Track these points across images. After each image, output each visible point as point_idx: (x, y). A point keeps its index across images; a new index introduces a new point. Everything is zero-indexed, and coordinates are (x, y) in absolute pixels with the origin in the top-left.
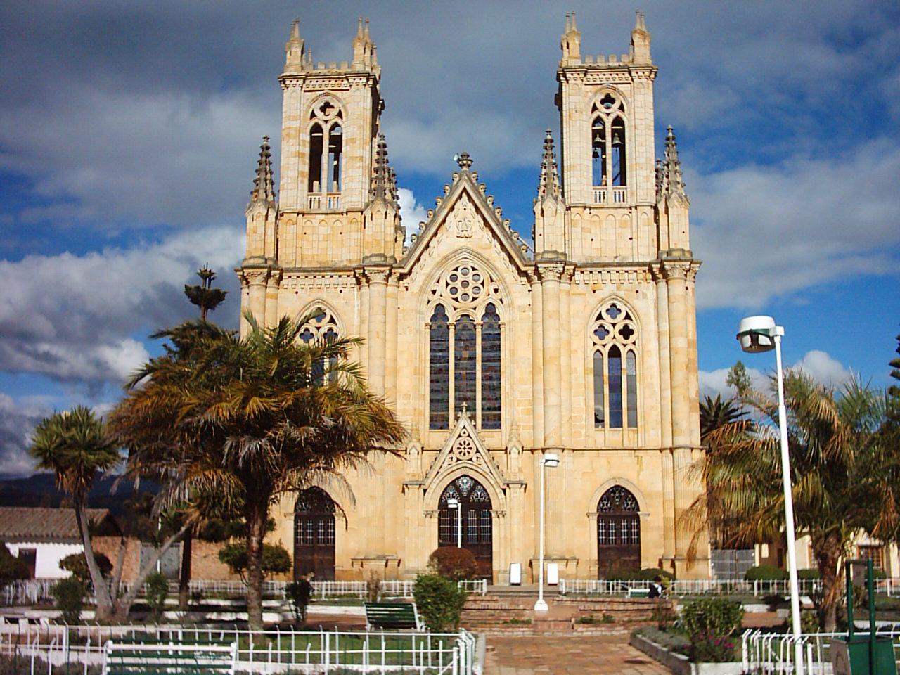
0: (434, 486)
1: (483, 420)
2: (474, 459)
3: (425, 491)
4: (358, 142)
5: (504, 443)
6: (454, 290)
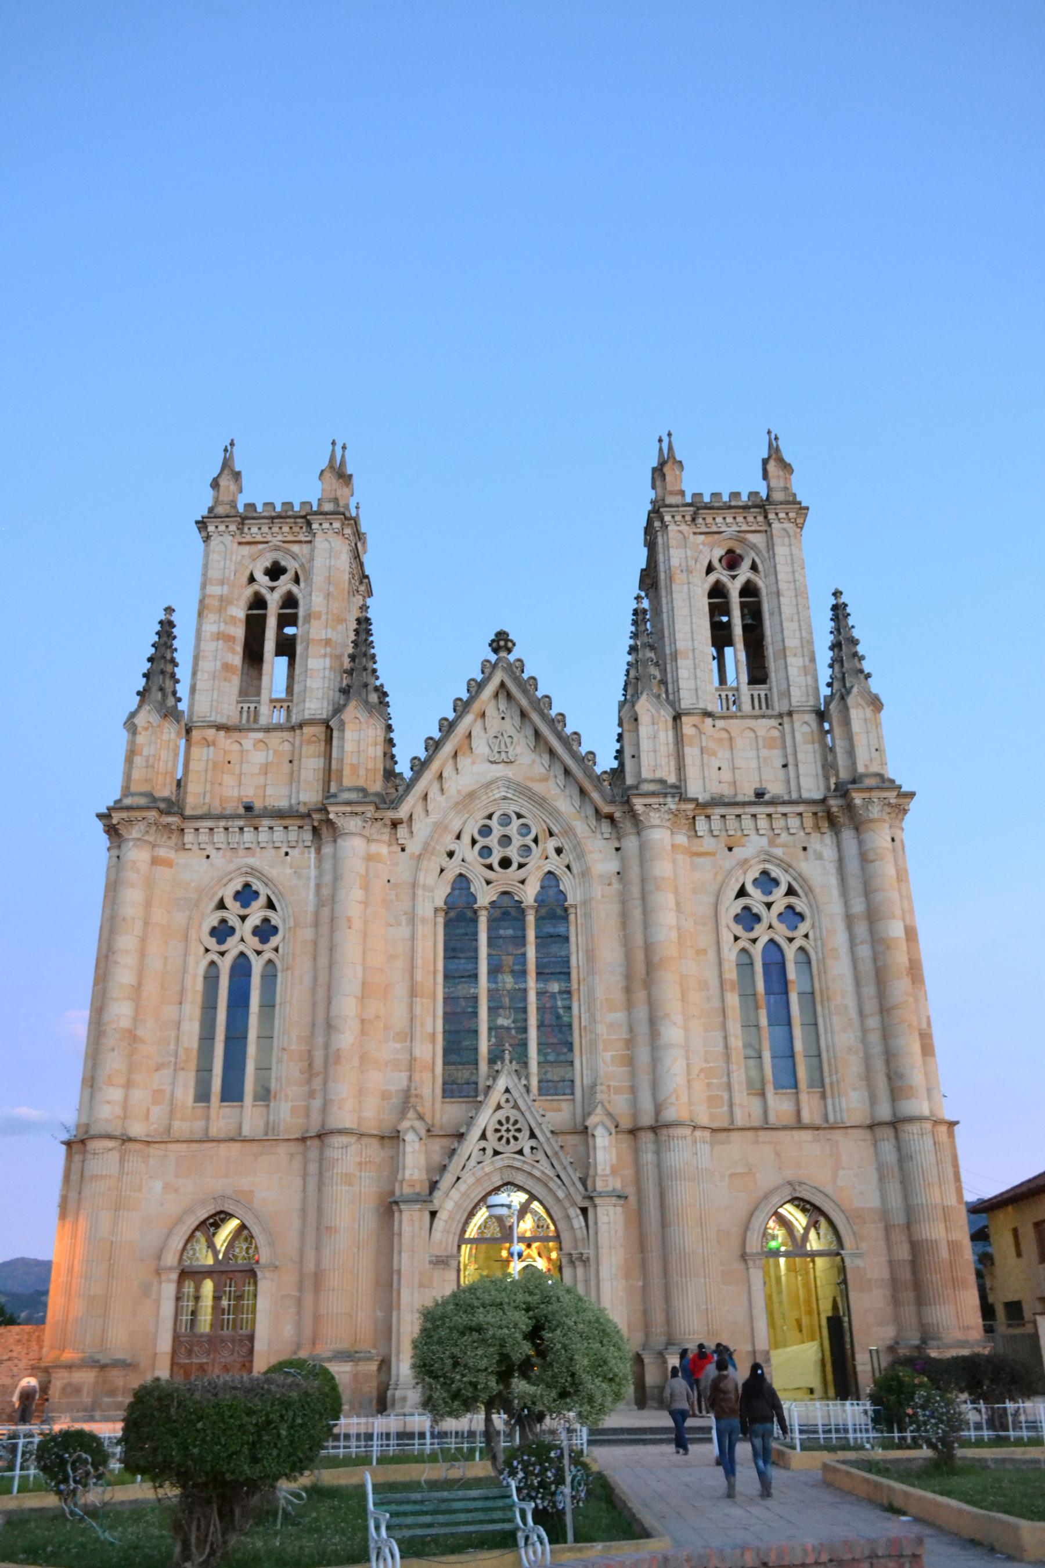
0: (449, 1205)
1: (524, 937)
2: (527, 1151)
3: (433, 1214)
4: (324, 617)
5: (579, 1119)
6: (486, 851)
